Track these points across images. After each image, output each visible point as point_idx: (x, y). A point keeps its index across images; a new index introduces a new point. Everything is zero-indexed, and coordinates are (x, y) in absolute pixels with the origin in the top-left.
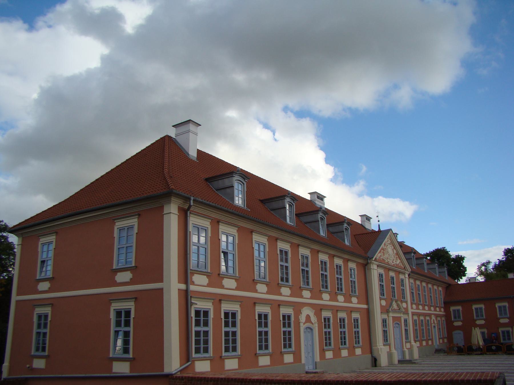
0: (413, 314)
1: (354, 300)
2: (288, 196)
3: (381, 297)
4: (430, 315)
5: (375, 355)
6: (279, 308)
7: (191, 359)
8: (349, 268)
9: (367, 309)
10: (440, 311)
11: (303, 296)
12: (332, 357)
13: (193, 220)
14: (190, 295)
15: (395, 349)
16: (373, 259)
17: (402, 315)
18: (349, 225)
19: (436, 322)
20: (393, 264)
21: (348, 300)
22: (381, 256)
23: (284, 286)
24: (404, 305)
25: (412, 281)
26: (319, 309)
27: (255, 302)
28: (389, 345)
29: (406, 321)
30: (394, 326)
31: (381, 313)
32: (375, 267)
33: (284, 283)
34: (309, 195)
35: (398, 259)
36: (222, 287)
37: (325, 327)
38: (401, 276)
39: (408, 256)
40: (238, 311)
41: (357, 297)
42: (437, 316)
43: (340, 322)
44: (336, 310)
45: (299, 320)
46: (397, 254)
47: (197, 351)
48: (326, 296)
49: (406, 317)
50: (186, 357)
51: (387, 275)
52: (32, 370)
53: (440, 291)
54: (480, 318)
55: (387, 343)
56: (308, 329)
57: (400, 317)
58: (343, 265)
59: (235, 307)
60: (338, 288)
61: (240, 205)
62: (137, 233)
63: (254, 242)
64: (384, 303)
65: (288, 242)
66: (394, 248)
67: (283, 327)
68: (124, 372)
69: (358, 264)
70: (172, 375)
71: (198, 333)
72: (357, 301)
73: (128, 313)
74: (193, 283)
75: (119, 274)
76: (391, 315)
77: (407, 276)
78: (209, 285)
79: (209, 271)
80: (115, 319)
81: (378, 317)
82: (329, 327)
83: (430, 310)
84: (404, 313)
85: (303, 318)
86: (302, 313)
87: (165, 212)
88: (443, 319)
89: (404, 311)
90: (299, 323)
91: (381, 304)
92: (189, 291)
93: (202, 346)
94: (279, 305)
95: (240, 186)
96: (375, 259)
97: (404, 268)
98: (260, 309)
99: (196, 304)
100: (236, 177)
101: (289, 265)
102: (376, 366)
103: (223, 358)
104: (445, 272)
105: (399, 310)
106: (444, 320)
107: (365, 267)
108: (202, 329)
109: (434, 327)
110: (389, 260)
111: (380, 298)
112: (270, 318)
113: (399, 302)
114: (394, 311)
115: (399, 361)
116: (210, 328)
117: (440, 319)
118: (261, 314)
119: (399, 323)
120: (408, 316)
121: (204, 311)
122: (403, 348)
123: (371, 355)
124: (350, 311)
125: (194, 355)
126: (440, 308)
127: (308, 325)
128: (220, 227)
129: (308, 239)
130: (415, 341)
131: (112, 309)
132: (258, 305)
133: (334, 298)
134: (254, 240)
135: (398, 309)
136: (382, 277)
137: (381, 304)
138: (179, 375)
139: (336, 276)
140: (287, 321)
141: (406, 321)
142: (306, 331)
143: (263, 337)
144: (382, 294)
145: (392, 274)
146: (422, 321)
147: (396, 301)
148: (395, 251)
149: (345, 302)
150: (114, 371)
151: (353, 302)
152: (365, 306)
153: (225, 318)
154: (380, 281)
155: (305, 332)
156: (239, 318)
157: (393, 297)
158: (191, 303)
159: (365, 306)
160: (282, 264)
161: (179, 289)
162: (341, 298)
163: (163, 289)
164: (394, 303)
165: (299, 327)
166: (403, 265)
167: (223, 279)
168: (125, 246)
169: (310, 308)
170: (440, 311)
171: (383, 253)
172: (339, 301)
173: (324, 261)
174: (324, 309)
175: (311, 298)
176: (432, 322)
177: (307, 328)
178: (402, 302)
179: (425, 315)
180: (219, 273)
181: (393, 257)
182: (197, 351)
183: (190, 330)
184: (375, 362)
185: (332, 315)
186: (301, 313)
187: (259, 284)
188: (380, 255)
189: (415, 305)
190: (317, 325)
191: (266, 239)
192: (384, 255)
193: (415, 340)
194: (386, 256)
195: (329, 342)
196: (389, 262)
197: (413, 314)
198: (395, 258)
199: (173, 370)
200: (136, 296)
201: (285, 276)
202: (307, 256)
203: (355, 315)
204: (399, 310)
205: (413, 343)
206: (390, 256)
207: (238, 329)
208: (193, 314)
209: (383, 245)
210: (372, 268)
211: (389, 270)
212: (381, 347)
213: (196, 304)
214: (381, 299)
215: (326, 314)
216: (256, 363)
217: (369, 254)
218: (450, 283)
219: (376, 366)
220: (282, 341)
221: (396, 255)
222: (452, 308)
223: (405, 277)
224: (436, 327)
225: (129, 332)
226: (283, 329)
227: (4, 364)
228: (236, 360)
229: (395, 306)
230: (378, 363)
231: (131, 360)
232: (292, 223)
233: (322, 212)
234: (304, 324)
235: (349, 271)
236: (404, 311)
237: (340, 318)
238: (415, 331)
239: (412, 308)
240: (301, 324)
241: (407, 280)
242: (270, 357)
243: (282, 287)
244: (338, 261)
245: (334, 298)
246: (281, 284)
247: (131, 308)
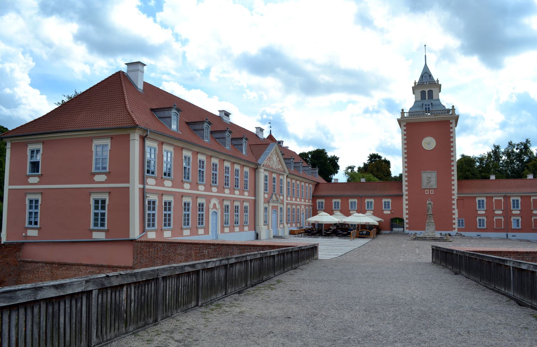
0: (287, 204)
1: (246, 193)
2: (173, 108)
3: (265, 192)
4: (300, 205)
5: (258, 231)
6: (223, 201)
7: (145, 231)
8: (244, 171)
9: (143, 189)
10: (309, 202)
11: (164, 185)
12: (203, 233)
13: (148, 143)
14: (146, 191)
15: (272, 228)
16: (262, 165)
17: (279, 205)
18: (230, 133)
19: (304, 210)
20: (276, 168)
21: (242, 193)
22: (267, 163)
23: (166, 179)
24: (281, 198)
25: (289, 180)
26: (222, 200)
27: (182, 195)
28: (268, 225)
29: (281, 209)
30: (273, 212)
31: (264, 203)
32: (262, 171)
33: (167, 177)
34: (219, 112)
35: (280, 165)
36: (164, 186)
37: (199, 211)
38: (281, 177)
39: (288, 161)
40: (172, 201)
41: (204, 185)
42: (305, 206)
43: (235, 208)
44: (234, 200)
45: (209, 207)
46: (280, 161)
47: (149, 226)
48: (227, 191)
49: (282, 206)
50: (143, 230)
51: (271, 176)
52: (26, 237)
53: (311, 188)
54: (353, 209)
55: (266, 224)
56: (214, 212)
57: (278, 206)
58: (218, 164)
59: (169, 198)
60: (225, 183)
61: (175, 130)
62: (110, 150)
63: (163, 151)
64: (266, 196)
65: (230, 161)
66: (278, 156)
67: (199, 211)
68: (102, 238)
69: (251, 168)
70: (135, 240)
71: (149, 214)
72: (190, 187)
73: (103, 202)
74: (147, 184)
75: (96, 176)
76: (271, 204)
77: (285, 177)
78: (156, 185)
79: (156, 176)
80: (94, 205)
81: (262, 205)
82: (202, 211)
83: (300, 201)
84: (280, 204)
85: (211, 206)
86: (211, 202)
87: (130, 139)
88: (311, 208)
89: (280, 202)
90: (209, 208)
91: (264, 197)
92: (145, 189)
93: (151, 223)
94: (197, 197)
95: (175, 116)
96: (263, 165)
97: (284, 171)
98: (186, 200)
99: (149, 197)
100: (174, 111)
101: (204, 170)
102: (257, 239)
103: (163, 230)
104: (316, 173)
105: (277, 201)
106: (311, 209)
107: (255, 170)
108: (152, 212)
109: (303, 213)
110: (273, 166)
111: (264, 192)
112: (191, 205)
113: (278, 196)
114: (274, 202)
115: (273, 236)
116: (156, 212)
117: (308, 208)
118: (167, 202)
119: (276, 210)
120: (283, 205)
121: (169, 202)
122: (278, 228)
123: (254, 231)
124: (244, 201)
125: (147, 228)
126: (309, 200)
127: (214, 210)
128: (164, 147)
129: (218, 152)
130: (287, 223)
131: (91, 198)
132: (165, 195)
133: (232, 192)
134: (163, 149)
135: (276, 200)
136: (275, 180)
137: (264, 197)
138: (139, 240)
139: (212, 172)
140: (201, 208)
141: (281, 209)
142: (213, 213)
143: (167, 218)
144: (266, 190)
145: (274, 175)
146: (294, 209)
147: (275, 195)
148: (278, 159)
149: (239, 195)
150: (93, 237)
151: (245, 195)
152: (253, 198)
153: (148, 205)
154: (265, 181)
155: (212, 215)
156: (173, 205)
157: (273, 192)
158: (146, 196)
159: (253, 198)
160: (213, 172)
161: (139, 188)
162: (237, 192)
163: (129, 188)
164: (274, 196)
165: (209, 211)
166: (283, 169)
167: (164, 181)
168: (101, 158)
169: (216, 199)
170: (309, 202)
171: (270, 160)
172: (236, 194)
173: (202, 160)
174: (185, 196)
175: (217, 192)
176: (302, 210)
177: (213, 212)
178: (280, 195)
179: (297, 205)
180: (161, 177)
181: (276, 163)
182: (149, 226)
183: (145, 213)
184: (257, 236)
185: (206, 202)
186: (210, 202)
187: (166, 181)
188: (267, 162)
189: (289, 198)
190: (220, 210)
191: (157, 144)
192: (270, 162)
193: (287, 223)
194: (272, 162)
195: (166, 221)
196: (273, 167)
197: (287, 204)
198: (278, 164)
199: (136, 237)
200: (110, 192)
201: (227, 182)
202: (189, 157)
203: (246, 204)
204: (277, 201)
205: (285, 224)
206: (274, 162)
207: (172, 212)
208: (147, 203)
209: (270, 154)
210: (260, 171)
211: (272, 172)
212: (262, 226)
213: (149, 197)
214: (264, 193)
215: (226, 203)
216: (182, 235)
217: (259, 162)
218: (319, 181)
219: (257, 239)
220: (183, 221)
221: (279, 162)
222: (318, 201)
223: (284, 178)
224: (304, 214)
225: (104, 213)
226: (184, 212)
227: (2, 233)
228: (189, 230)
229: (274, 198)
230: (259, 236)
231: (107, 231)
232: (207, 140)
233: (207, 123)
234: (212, 209)
235: (244, 173)
236: (280, 202)
237: (165, 201)
238: (288, 215)
239: (287, 200)
240: (210, 210)
241: (285, 180)
242: (156, 233)
243: (148, 178)
244: (237, 167)
245: (232, 192)
246: (164, 178)
247: (106, 199)
